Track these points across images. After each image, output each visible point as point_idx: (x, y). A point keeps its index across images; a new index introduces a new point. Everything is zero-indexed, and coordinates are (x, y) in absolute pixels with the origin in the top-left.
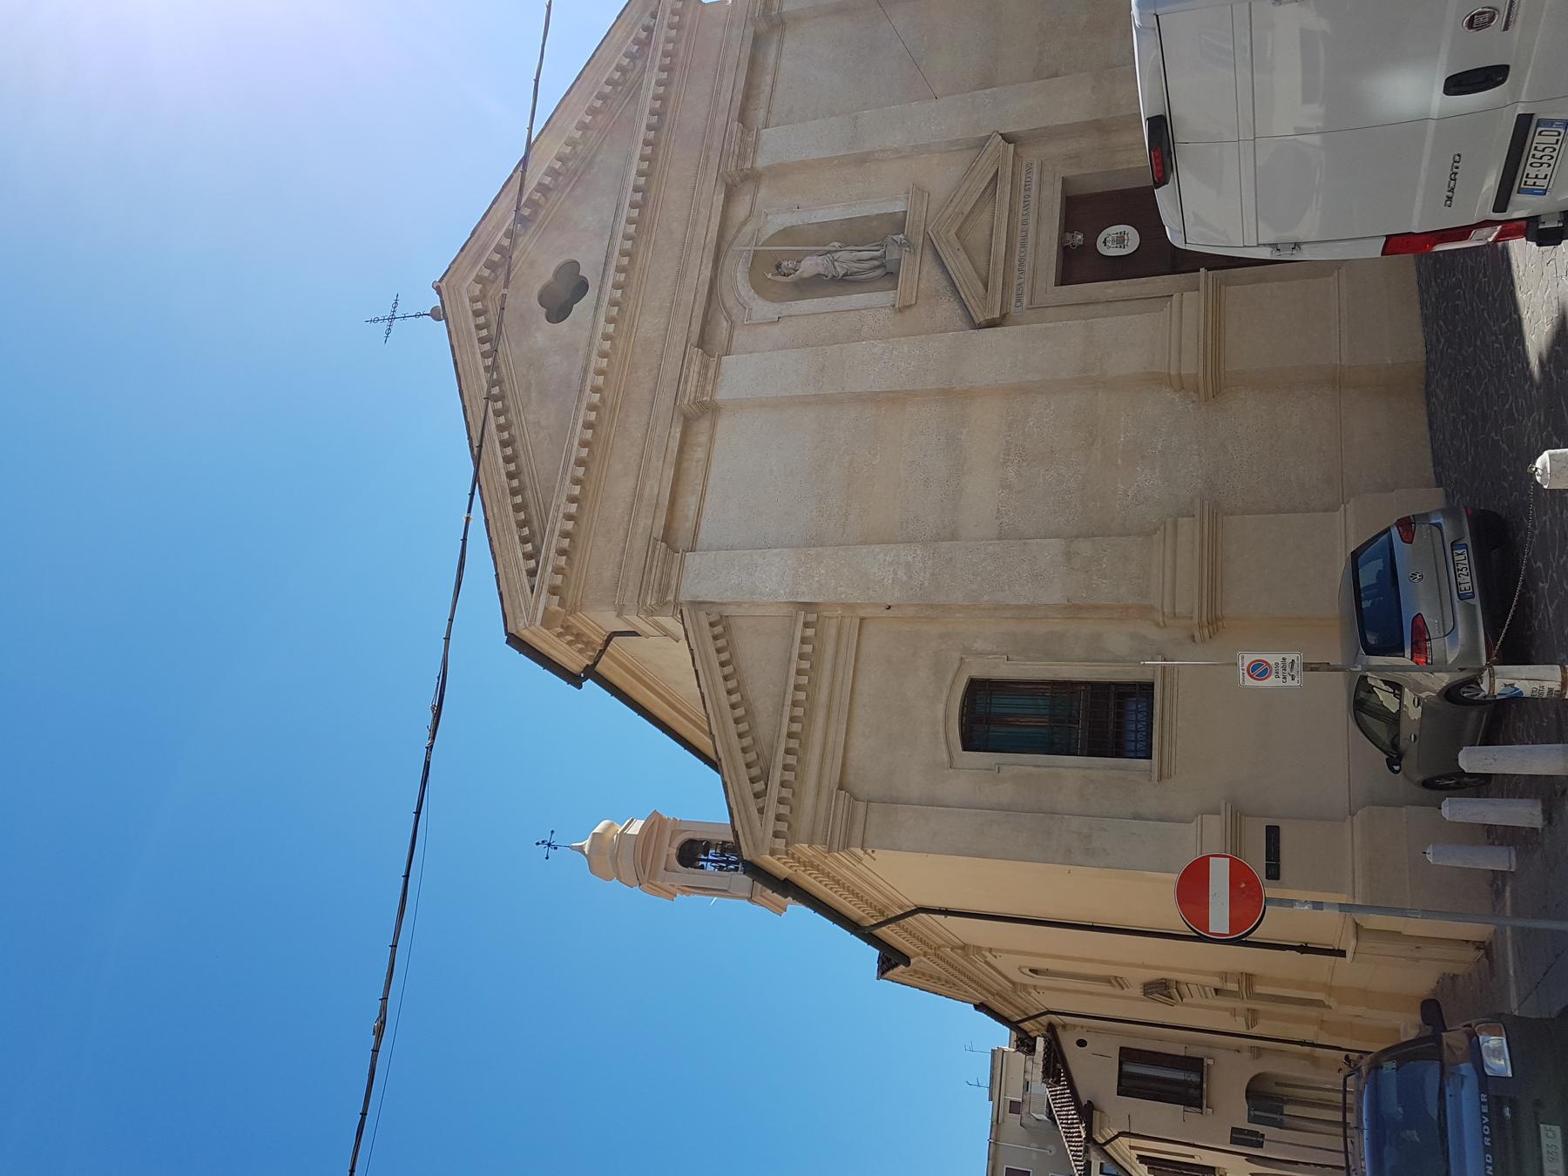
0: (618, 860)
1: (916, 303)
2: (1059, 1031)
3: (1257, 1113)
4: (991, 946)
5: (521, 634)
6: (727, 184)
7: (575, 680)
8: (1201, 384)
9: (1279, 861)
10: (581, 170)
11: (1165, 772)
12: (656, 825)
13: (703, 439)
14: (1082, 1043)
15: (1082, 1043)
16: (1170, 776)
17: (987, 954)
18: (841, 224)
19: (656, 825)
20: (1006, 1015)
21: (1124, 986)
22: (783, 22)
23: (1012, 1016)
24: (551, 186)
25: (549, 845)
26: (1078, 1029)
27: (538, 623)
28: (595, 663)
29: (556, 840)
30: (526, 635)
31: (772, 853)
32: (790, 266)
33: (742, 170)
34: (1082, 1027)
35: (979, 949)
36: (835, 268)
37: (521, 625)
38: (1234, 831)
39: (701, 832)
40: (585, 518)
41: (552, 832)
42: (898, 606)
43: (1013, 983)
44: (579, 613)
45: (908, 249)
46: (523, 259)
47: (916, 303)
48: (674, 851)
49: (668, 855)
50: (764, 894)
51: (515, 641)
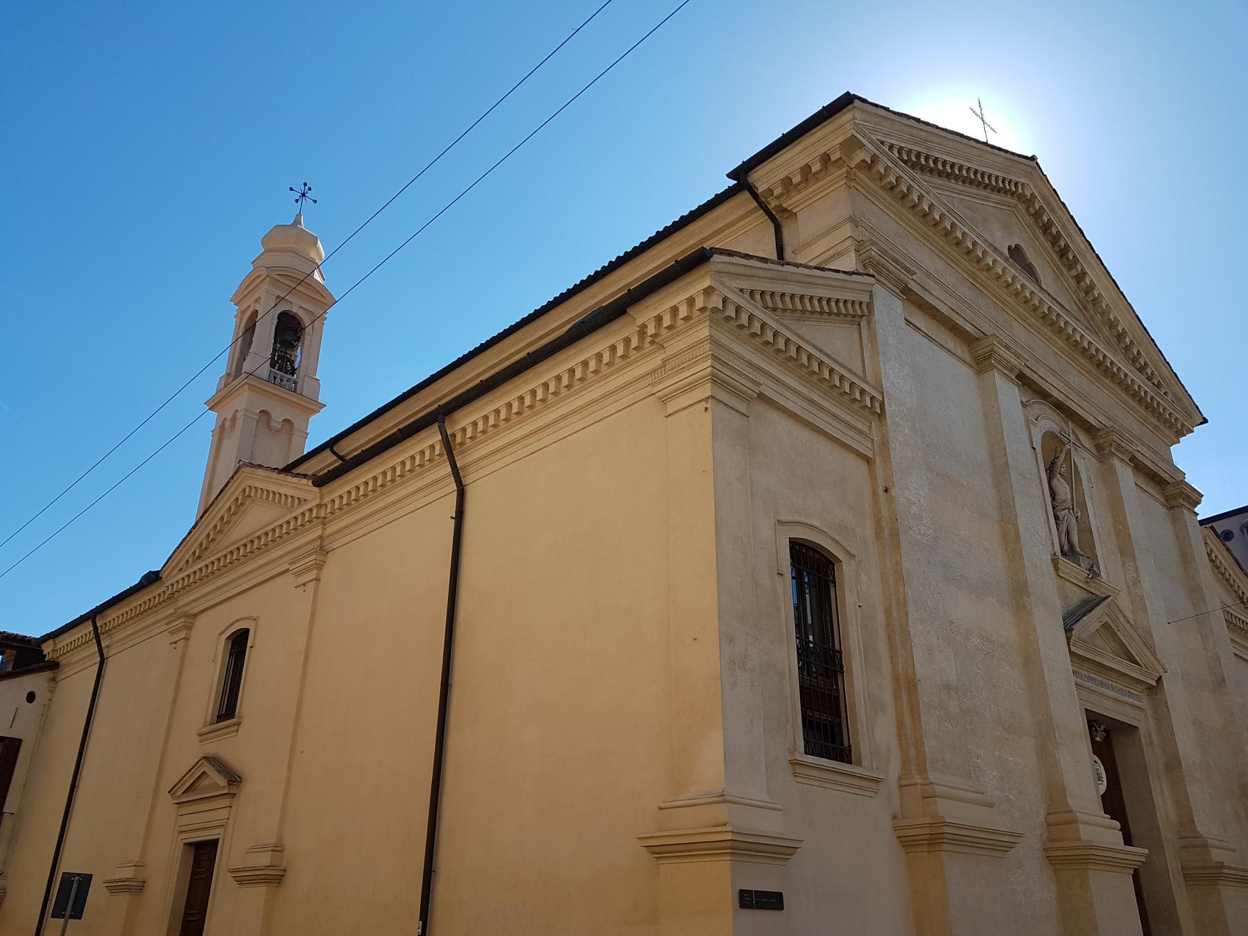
0: (291, 254)
1: (1059, 575)
2: (48, 674)
3: (75, 885)
4: (322, 582)
5: (849, 111)
6: (1099, 430)
7: (742, 175)
8: (1057, 845)
9: (758, 908)
10: (1086, 314)
11: (799, 769)
12: (323, 300)
13: (959, 352)
14: (31, 697)
15: (31, 697)
16: (795, 775)
17: (313, 574)
18: (1085, 523)
19: (323, 300)
20: (110, 611)
21: (203, 737)
22: (1172, 508)
23: (103, 618)
24: (1082, 283)
25: (303, 195)
26: (49, 695)
27: (855, 133)
28: (755, 196)
29: (307, 203)
30: (845, 117)
31: (708, 291)
32: (1063, 469)
33: (1111, 446)
34: (50, 700)
35: (320, 567)
36: (1064, 509)
37: (857, 114)
38: (744, 846)
39: (311, 341)
40: (912, 217)
41: (315, 201)
42: (891, 500)
43: (195, 616)
44: (844, 181)
45: (1090, 576)
46: (1037, 243)
47: (1059, 575)
48: (295, 309)
49: (291, 302)
50: (246, 386)
51: (847, 100)
